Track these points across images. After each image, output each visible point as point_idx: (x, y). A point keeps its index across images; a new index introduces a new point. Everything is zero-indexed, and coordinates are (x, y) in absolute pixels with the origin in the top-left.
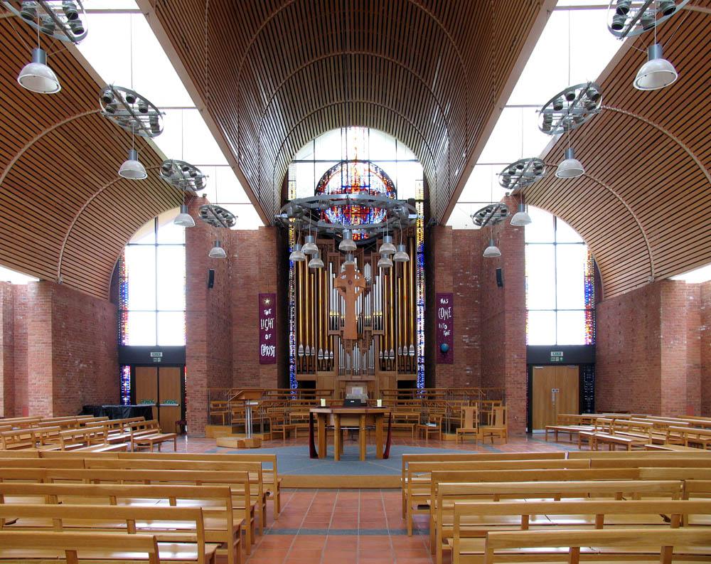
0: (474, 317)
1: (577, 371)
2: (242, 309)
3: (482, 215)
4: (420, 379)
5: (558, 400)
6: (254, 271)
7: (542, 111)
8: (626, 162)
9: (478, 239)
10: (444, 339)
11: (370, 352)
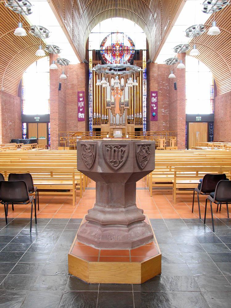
0: (166, 101)
1: (207, 124)
2: (70, 98)
3: (177, 49)
4: (144, 128)
5: (199, 137)
6: (75, 82)
7: (203, 4)
8: (221, 44)
9: (171, 65)
10: (154, 111)
11: (123, 116)
